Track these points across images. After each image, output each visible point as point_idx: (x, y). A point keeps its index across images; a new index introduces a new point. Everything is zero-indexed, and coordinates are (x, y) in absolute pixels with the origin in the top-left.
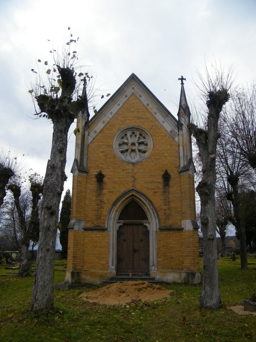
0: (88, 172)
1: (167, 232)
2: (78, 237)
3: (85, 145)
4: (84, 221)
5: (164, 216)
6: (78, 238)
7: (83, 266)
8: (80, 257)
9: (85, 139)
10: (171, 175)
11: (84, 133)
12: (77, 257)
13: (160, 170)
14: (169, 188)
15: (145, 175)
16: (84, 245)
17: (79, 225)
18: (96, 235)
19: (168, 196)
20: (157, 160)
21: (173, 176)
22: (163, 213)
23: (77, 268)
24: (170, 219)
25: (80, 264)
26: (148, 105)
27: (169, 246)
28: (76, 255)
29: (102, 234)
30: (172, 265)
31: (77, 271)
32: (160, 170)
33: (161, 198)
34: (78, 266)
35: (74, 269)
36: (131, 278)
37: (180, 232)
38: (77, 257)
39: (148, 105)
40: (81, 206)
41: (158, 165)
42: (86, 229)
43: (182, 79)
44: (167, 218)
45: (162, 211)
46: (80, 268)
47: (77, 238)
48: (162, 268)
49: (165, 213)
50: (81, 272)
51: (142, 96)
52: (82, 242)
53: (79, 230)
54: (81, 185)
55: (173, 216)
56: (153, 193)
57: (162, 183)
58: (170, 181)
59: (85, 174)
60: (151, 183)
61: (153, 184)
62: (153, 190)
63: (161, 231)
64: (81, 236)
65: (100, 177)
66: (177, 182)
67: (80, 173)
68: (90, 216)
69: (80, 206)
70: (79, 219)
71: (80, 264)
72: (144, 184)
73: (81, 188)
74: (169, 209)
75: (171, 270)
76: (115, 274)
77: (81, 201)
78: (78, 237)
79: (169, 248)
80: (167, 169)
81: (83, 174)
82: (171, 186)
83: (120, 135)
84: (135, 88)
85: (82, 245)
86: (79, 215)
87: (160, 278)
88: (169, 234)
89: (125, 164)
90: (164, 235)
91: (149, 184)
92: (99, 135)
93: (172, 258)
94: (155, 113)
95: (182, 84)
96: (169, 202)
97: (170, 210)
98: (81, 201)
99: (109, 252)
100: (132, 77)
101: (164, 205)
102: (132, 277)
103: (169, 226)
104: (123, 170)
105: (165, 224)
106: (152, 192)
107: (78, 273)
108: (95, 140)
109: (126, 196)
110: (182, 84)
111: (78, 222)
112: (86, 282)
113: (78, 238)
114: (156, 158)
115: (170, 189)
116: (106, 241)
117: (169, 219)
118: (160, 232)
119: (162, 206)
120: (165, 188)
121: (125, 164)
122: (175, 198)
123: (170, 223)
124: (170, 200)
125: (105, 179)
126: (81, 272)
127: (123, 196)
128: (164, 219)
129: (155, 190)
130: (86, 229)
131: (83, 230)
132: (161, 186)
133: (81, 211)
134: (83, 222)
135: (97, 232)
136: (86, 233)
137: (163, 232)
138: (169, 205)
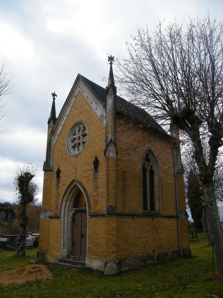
0: (52, 171)
1: (95, 218)
2: (44, 224)
3: (51, 148)
4: (50, 211)
5: (93, 202)
6: (43, 225)
7: (48, 248)
8: (46, 241)
9: (52, 143)
10: (100, 160)
11: (51, 139)
12: (43, 240)
13: (92, 157)
14: (98, 174)
15: (82, 165)
16: (49, 230)
17: (45, 215)
18: (55, 221)
19: (97, 182)
20: (91, 147)
21: (101, 161)
22: (93, 199)
23: (43, 249)
24: (98, 205)
25: (45, 246)
26: (87, 97)
27: (97, 232)
28: (42, 239)
29: (58, 221)
30: (98, 251)
31: (43, 251)
32: (92, 157)
33: (91, 185)
34: (44, 248)
35: (40, 250)
36: (71, 262)
37: (58, 219)
38: (43, 240)
39: (87, 97)
40: (47, 199)
41: (91, 153)
42: (51, 217)
43: (54, 95)
44: (96, 204)
45: (92, 198)
46: (46, 249)
47: (43, 225)
48: (91, 254)
49: (94, 200)
50: (46, 253)
51: (85, 91)
52: (47, 228)
53: (45, 218)
54: (47, 182)
55: (100, 202)
56: (87, 180)
57: (93, 169)
58: (99, 166)
59: (51, 172)
60: (86, 171)
61: (87, 172)
62: (87, 178)
63: (91, 217)
64: (46, 224)
65: (58, 172)
66: (104, 167)
67: (46, 173)
68: (53, 207)
69: (46, 199)
70: (45, 209)
71: (45, 246)
72: (82, 174)
73: (47, 184)
74: (97, 194)
75: (97, 257)
76: (66, 257)
77: (47, 195)
78: (44, 224)
79: (96, 234)
80: (96, 155)
81: (49, 173)
82: (99, 171)
83: (71, 132)
84: (81, 86)
85: (47, 231)
86: (45, 207)
87: (88, 263)
88: (96, 220)
89: (71, 158)
90: (93, 222)
91: (85, 173)
92: (59, 137)
93: (98, 245)
94: (92, 103)
95: (54, 99)
96: (97, 187)
97: (98, 196)
98: (47, 195)
99: (61, 238)
100: (78, 77)
101: (94, 191)
102: (73, 261)
103: (96, 212)
104: (71, 164)
105: (94, 211)
106: (86, 180)
107: (43, 254)
108: (57, 143)
109: (72, 187)
110: (54, 99)
111: (44, 212)
112: (49, 262)
113: (43, 225)
114: (90, 146)
115: (99, 174)
116: (151, 226)
117: (97, 205)
118: (91, 218)
119: (93, 193)
120: (95, 174)
121: (71, 158)
122: (101, 184)
123: (98, 209)
124: (98, 186)
125: (61, 174)
126: (46, 253)
127: (69, 187)
128: (94, 206)
129: (89, 178)
130: (51, 217)
131: (48, 218)
132: (92, 173)
133: (46, 203)
134: (48, 211)
135: (56, 219)
136: (52, 220)
137: (93, 218)
138: (97, 191)
